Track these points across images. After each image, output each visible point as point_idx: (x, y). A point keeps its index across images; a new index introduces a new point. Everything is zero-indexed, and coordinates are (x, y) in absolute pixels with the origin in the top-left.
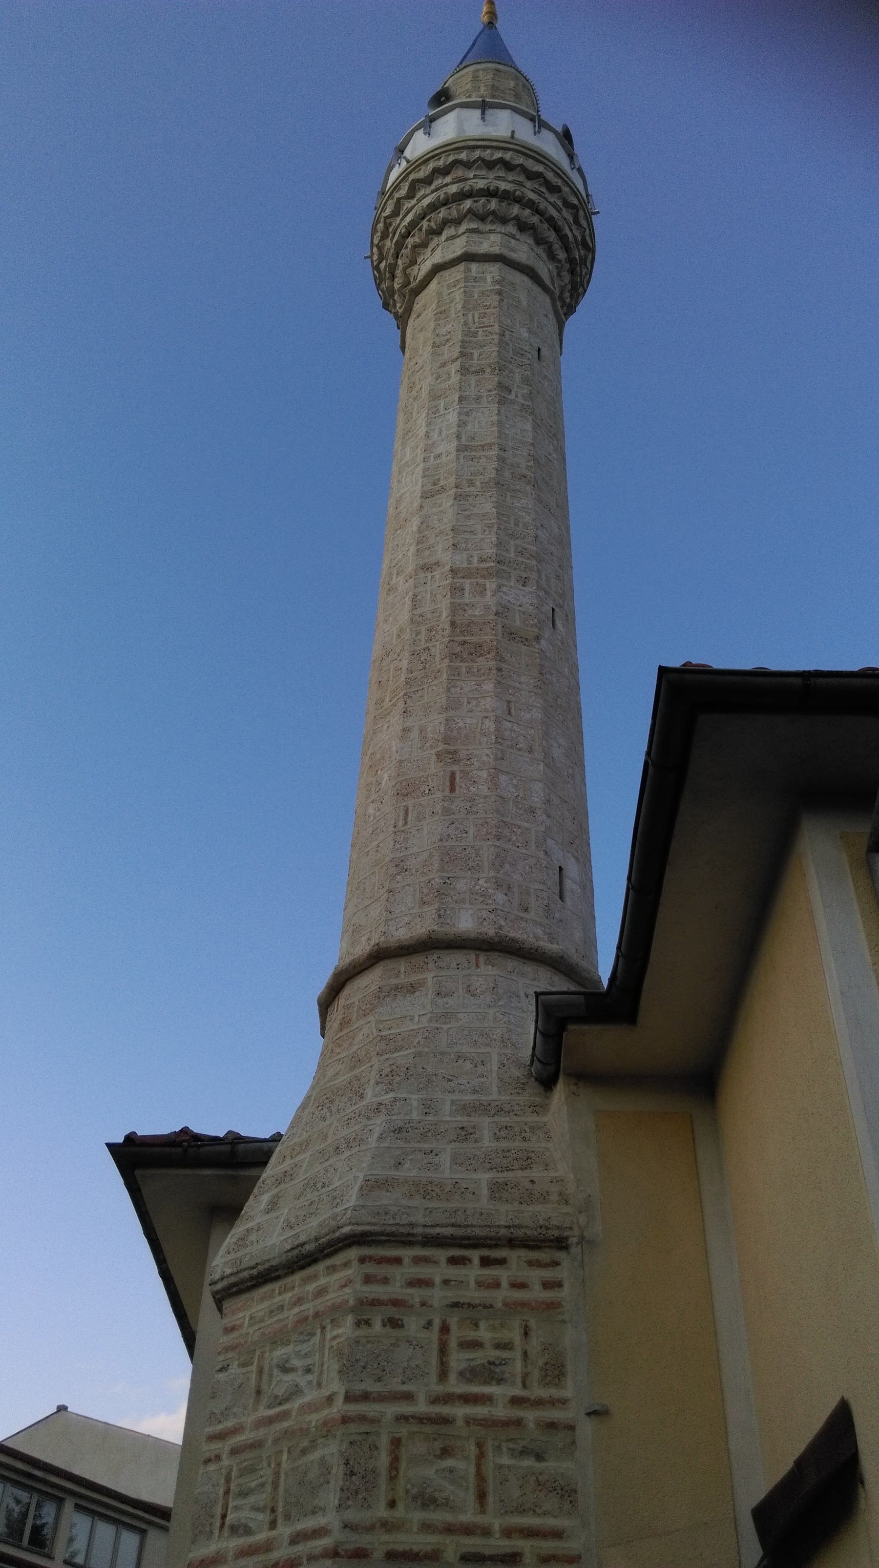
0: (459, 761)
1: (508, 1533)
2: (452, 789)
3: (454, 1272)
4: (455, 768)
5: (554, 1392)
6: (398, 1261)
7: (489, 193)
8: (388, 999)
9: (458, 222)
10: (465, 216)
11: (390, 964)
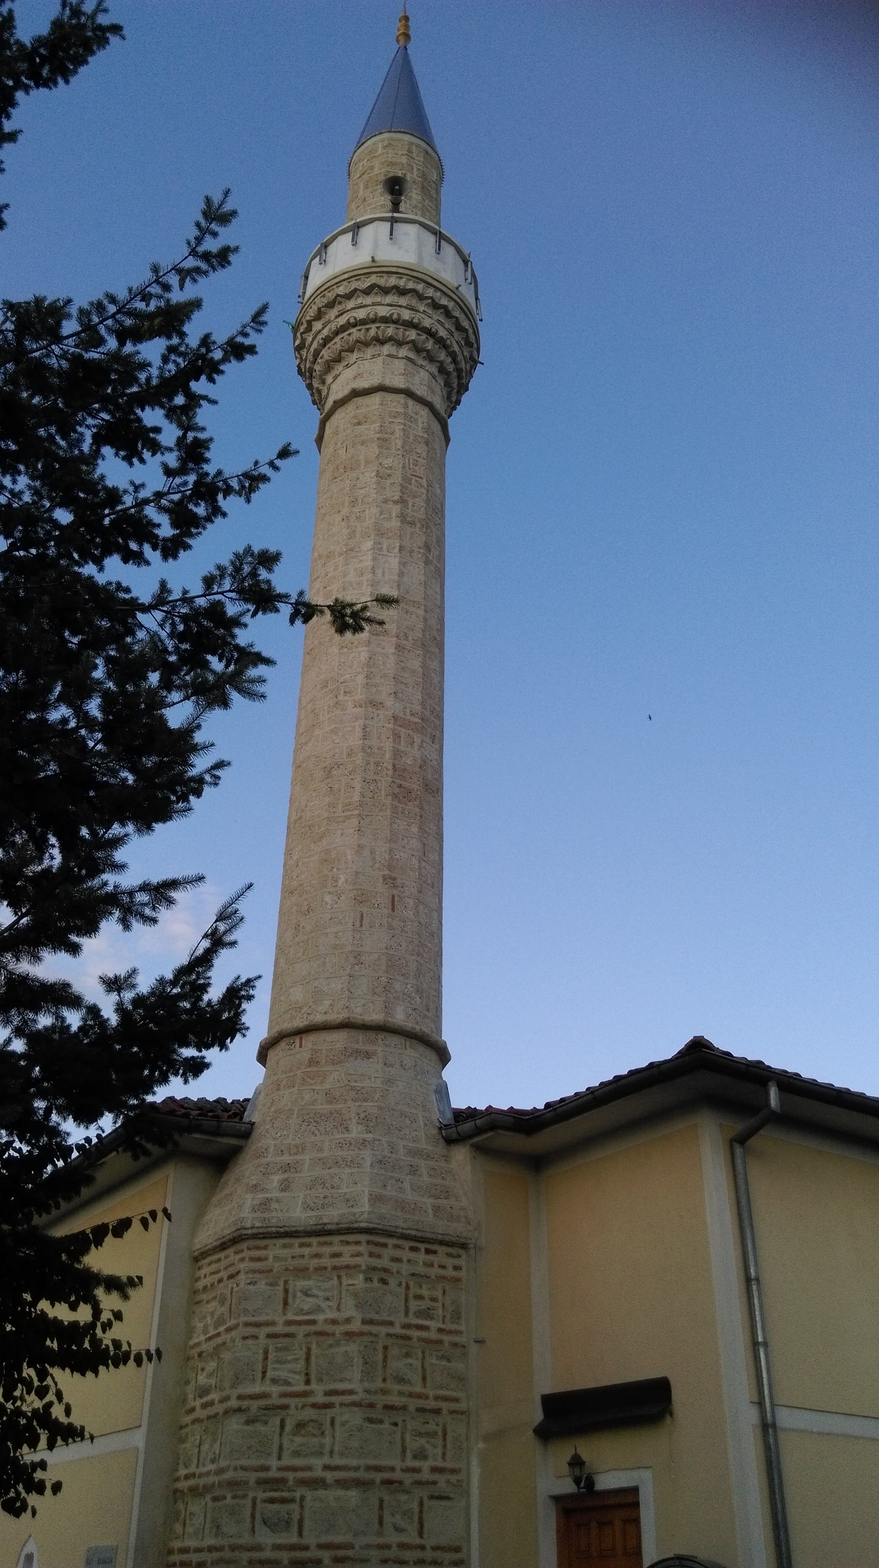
0: (398, 887)
1: (436, 1398)
2: (393, 910)
3: (412, 1255)
4: (395, 892)
5: (453, 1327)
6: (385, 1245)
7: (430, 333)
8: (352, 1058)
9: (400, 344)
10: (408, 343)
11: (353, 1033)
